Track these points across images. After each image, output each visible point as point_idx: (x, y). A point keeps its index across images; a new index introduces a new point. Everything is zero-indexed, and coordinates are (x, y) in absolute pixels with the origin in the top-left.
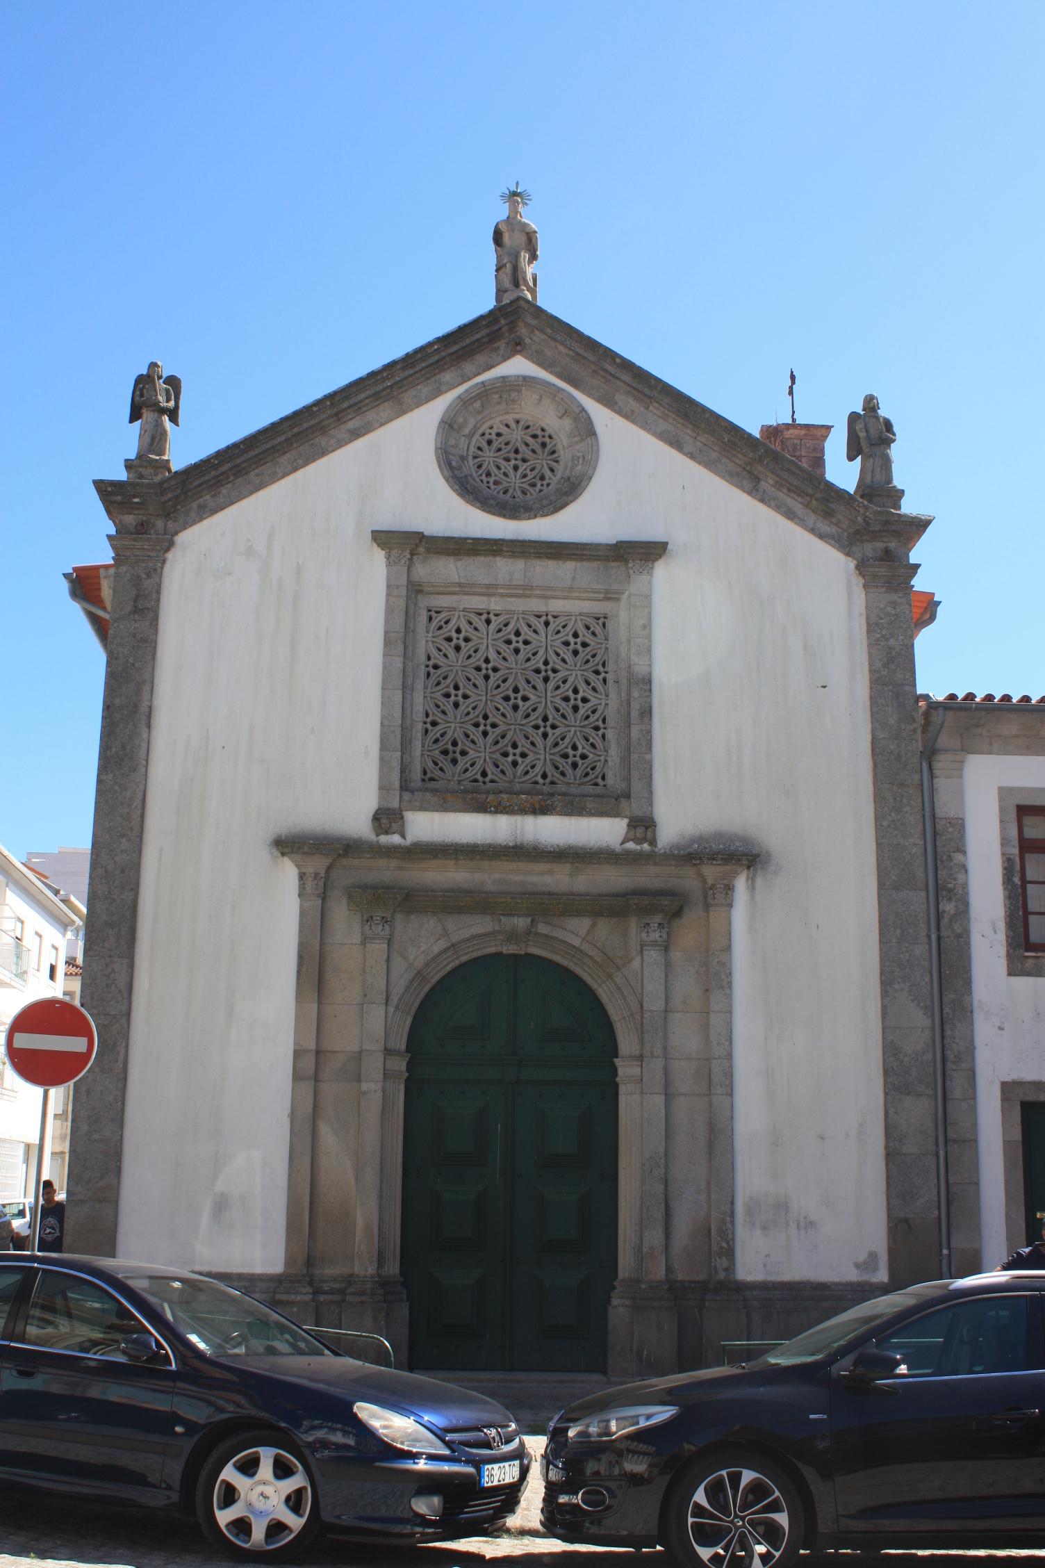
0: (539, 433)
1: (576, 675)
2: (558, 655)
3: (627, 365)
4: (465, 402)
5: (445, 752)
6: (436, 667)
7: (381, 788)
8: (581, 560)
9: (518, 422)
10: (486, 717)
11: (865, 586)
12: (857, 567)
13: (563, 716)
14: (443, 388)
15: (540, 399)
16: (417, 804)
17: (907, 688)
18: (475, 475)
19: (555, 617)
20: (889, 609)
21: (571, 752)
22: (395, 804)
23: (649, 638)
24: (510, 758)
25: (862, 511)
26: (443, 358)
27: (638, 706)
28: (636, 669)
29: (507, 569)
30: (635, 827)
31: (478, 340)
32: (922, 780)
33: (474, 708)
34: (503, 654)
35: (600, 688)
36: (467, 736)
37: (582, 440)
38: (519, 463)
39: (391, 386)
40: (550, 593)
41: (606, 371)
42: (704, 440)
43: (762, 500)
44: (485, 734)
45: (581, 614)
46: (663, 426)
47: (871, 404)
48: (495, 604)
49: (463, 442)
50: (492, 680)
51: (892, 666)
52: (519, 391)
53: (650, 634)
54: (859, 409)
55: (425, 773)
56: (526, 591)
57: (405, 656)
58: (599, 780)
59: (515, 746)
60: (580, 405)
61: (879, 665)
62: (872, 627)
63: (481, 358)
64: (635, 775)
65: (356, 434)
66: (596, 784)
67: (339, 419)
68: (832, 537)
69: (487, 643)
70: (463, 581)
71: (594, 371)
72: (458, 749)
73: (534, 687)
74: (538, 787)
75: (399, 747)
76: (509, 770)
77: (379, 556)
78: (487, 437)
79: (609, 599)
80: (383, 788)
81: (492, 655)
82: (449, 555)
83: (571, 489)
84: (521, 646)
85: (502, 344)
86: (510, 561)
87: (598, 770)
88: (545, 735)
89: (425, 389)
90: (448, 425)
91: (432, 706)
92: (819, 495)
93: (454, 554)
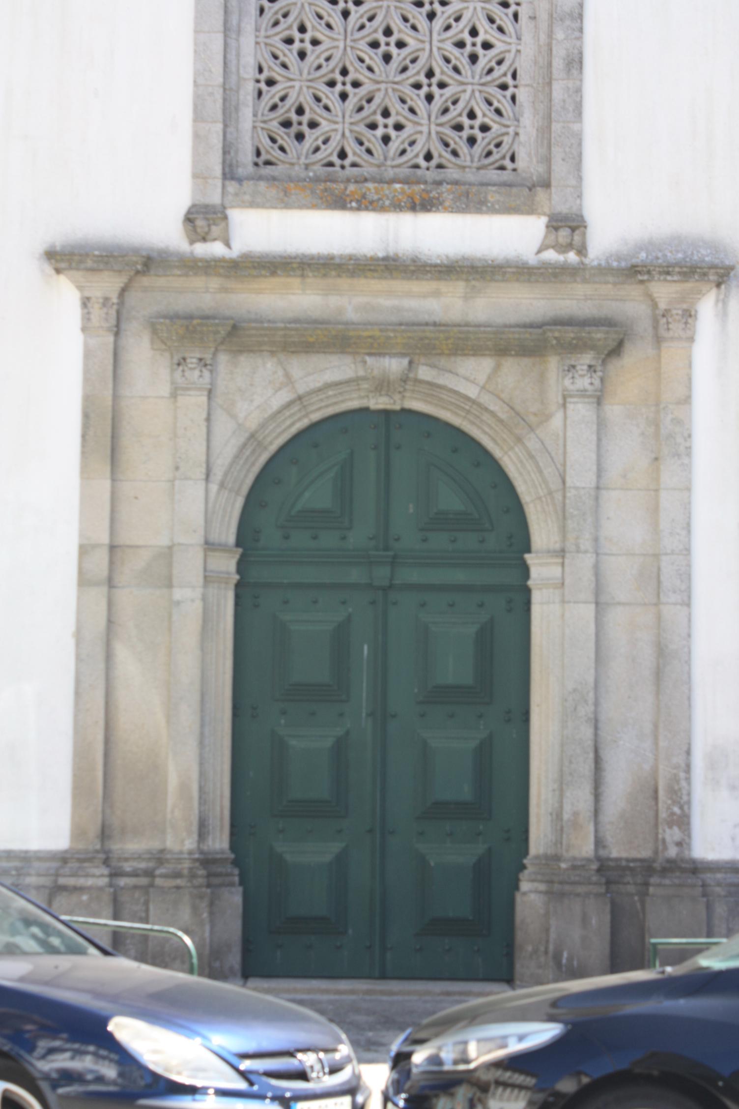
5: (287, 124)
7: (195, 176)
16: (247, 198)
22: (215, 198)
24: (380, 132)
30: (556, 229)
35: (508, 25)
55: (258, 154)
58: (507, 162)
59: (386, 114)
66: (502, 168)
74: (419, 172)
75: (220, 116)
76: (377, 147)
80: (199, 176)
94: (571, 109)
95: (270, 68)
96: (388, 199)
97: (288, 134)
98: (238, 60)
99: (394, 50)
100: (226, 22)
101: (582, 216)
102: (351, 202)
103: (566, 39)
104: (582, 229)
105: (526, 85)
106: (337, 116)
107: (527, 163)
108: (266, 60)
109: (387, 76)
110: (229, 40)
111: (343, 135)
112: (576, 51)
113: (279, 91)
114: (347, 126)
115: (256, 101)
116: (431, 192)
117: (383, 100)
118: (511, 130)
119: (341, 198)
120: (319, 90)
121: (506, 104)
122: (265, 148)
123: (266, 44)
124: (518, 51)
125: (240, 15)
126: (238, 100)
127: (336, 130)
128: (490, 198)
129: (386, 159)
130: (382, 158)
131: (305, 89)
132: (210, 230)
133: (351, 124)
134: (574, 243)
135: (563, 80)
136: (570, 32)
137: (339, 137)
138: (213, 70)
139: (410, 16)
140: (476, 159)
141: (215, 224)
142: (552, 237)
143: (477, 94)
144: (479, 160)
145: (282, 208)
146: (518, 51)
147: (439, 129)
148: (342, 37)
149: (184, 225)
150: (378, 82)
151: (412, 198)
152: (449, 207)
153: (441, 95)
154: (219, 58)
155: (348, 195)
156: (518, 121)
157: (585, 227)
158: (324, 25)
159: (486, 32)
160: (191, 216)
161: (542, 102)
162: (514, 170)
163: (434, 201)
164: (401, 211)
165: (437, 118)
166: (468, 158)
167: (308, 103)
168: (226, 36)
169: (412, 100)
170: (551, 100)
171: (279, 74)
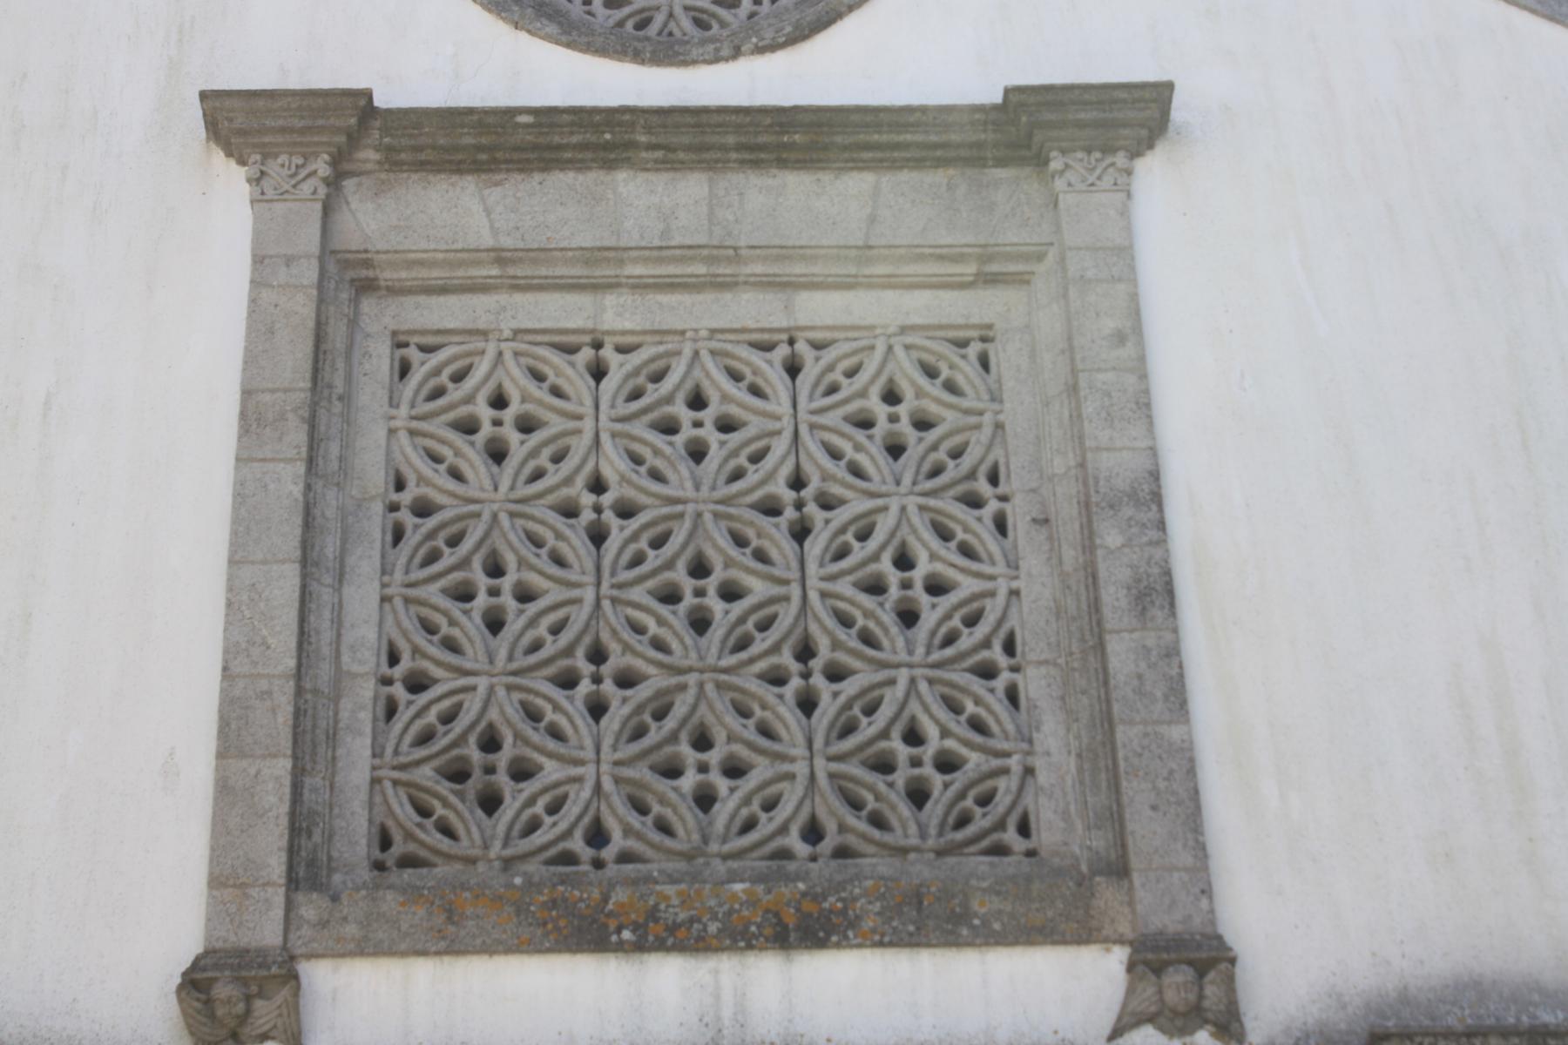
1: (900, 506)
5: (458, 774)
6: (423, 509)
7: (216, 882)
8: (895, 165)
10: (598, 655)
16: (351, 930)
19: (818, 346)
21: (902, 751)
22: (268, 932)
23: (1140, 368)
24: (689, 781)
27: (1124, 574)
28: (1105, 463)
30: (1158, 970)
33: (556, 630)
34: (651, 460)
35: (988, 541)
36: (534, 716)
44: (597, 709)
45: (903, 330)
48: (617, 314)
53: (1142, 358)
55: (385, 842)
57: (311, 462)
58: (1010, 836)
59: (702, 742)
64: (1136, 792)
66: (1000, 850)
69: (596, 432)
70: (507, 242)
72: (503, 759)
73: (761, 556)
74: (792, 867)
75: (286, 743)
77: (230, 182)
79: (992, 280)
80: (226, 880)
81: (613, 465)
82: (459, 169)
84: (710, 434)
86: (660, 180)
87: (1002, 802)
88: (807, 704)
91: (410, 625)
93: (477, 168)
94: (1159, 694)
95: (416, 651)
96: (714, 917)
100: (306, 545)
101: (1219, 938)
102: (619, 931)
103: (1128, 543)
104: (1223, 966)
105: (1040, 663)
106: (582, 748)
107: (1060, 827)
108: (405, 634)
109: (701, 658)
110: (314, 586)
111: (598, 788)
112: (1156, 570)
114: (604, 767)
117: (694, 708)
118: (1014, 762)
119: (594, 921)
121: (986, 536)
122: (400, 825)
123: (407, 601)
124: (1015, 593)
127: (578, 780)
128: (975, 905)
129: (705, 840)
130: (696, 837)
131: (501, 692)
132: (248, 1012)
133: (617, 763)
134: (1206, 1004)
135: (1132, 631)
136: (1134, 530)
137: (586, 793)
138: (271, 641)
139: (750, 533)
140: (933, 831)
141: (260, 995)
142: (1148, 990)
143: (923, 687)
144: (940, 834)
146: (1015, 593)
147: (835, 767)
148: (590, 578)
149: (180, 1001)
150: (680, 671)
151: (777, 914)
152: (874, 931)
153: (836, 695)
154: (290, 616)
155: (610, 915)
156: (1031, 742)
157: (1233, 961)
158: (545, 558)
159: (933, 557)
160: (198, 976)
161: (1084, 692)
162: (1031, 853)
164: (750, 947)
165: (827, 743)
166: (913, 829)
168: (305, 577)
170: (1106, 683)
171: (439, 663)
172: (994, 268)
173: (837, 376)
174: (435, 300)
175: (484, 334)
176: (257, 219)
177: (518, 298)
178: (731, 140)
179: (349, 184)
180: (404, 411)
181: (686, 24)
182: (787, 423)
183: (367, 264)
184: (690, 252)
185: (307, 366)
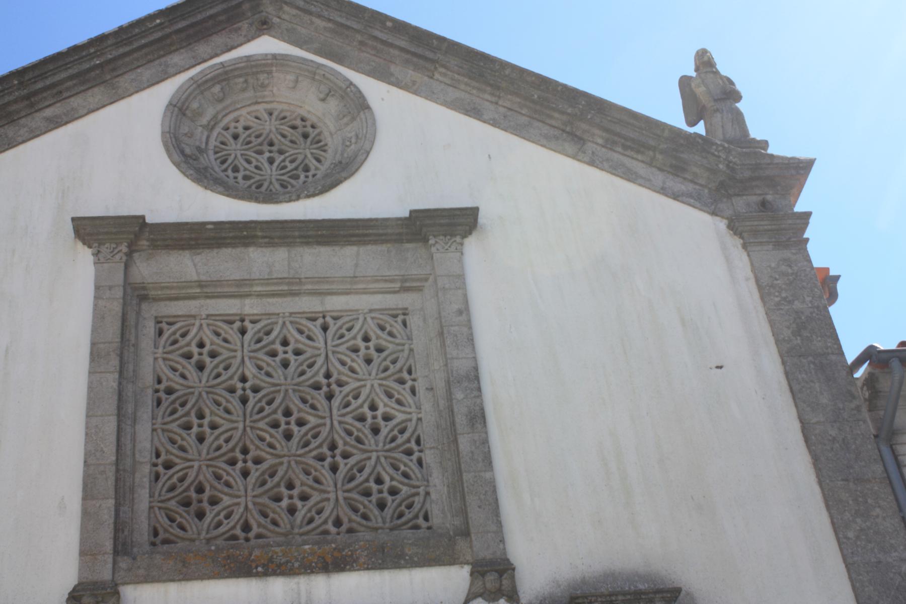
0: (298, 122)
1: (370, 383)
2: (343, 364)
3: (401, 27)
4: (200, 86)
5: (186, 504)
6: (169, 391)
7: (82, 553)
9: (271, 114)
11: (745, 246)
12: (730, 227)
13: (359, 440)
14: (171, 70)
15: (297, 81)
16: (142, 572)
17: (833, 358)
18: (217, 169)
20: (783, 268)
24: (285, 503)
25: (723, 155)
26: (168, 36)
29: (262, 261)
30: (483, 574)
31: (211, 17)
32: (886, 470)
35: (408, 398)
36: (218, 477)
37: (353, 119)
38: (275, 155)
39: (101, 66)
40: (326, 287)
41: (376, 38)
42: (508, 104)
43: (592, 163)
44: (245, 474)
45: (371, 311)
46: (453, 94)
47: (704, 62)
48: (250, 307)
49: (200, 135)
50: (250, 404)
51: (806, 334)
52: (270, 73)
53: (469, 321)
54: (832, 273)
55: (156, 533)
56: (292, 287)
57: (121, 373)
58: (421, 521)
59: (290, 486)
60: (346, 79)
61: (787, 333)
62: (765, 291)
63: (218, 40)
65: (56, 123)
66: (416, 527)
67: (32, 105)
68: (690, 196)
70: (203, 278)
71: (362, 43)
72: (205, 496)
73: (313, 407)
74: (329, 537)
75: (112, 492)
76: (284, 519)
77: (85, 255)
78: (232, 130)
80: (87, 552)
81: (250, 370)
82: (182, 248)
83: (344, 169)
84: (291, 357)
85: (244, 25)
86: (267, 251)
87: (417, 507)
89: (146, 73)
90: (179, 109)
92: (663, 146)
95: (167, 452)
96: (297, 560)
97: (188, 513)
98: (134, 446)
99: (291, 357)
100: (119, 408)
101: (508, 560)
102: (256, 568)
104: (510, 572)
105: (431, 448)
106: (239, 490)
108: (163, 444)
109: (289, 451)
111: (246, 507)
113: (178, 472)
114: (249, 498)
115: (153, 483)
116: (343, 550)
118: (421, 490)
120: (219, 468)
123: (163, 430)
124: (420, 419)
125: (136, 406)
126: (134, 483)
127: (238, 504)
128: (407, 551)
129: (292, 528)
130: (288, 526)
131: (204, 468)
133: (254, 496)
137: (241, 509)
138: (105, 449)
140: (388, 520)
143: (383, 460)
144: (391, 522)
145: (179, 580)
146: (420, 419)
148: (241, 419)
151: (323, 558)
152: (364, 563)
153: (346, 464)
154: (113, 438)
155: (253, 561)
156: (428, 481)
157: (514, 569)
159: (385, 405)
161: (449, 460)
162: (429, 528)
163: (348, 560)
164: (312, 572)
165: (343, 485)
166: (380, 520)
167: (208, 481)
169: (316, 470)
171: (177, 457)
172: (408, 284)
173: (343, 331)
174: (173, 303)
175: (194, 317)
176: (97, 271)
177: (209, 301)
178: (297, 234)
179: (136, 255)
180: (160, 350)
181: (277, 186)
182: (323, 351)
183: (144, 288)
184: (281, 280)
185: (119, 332)
